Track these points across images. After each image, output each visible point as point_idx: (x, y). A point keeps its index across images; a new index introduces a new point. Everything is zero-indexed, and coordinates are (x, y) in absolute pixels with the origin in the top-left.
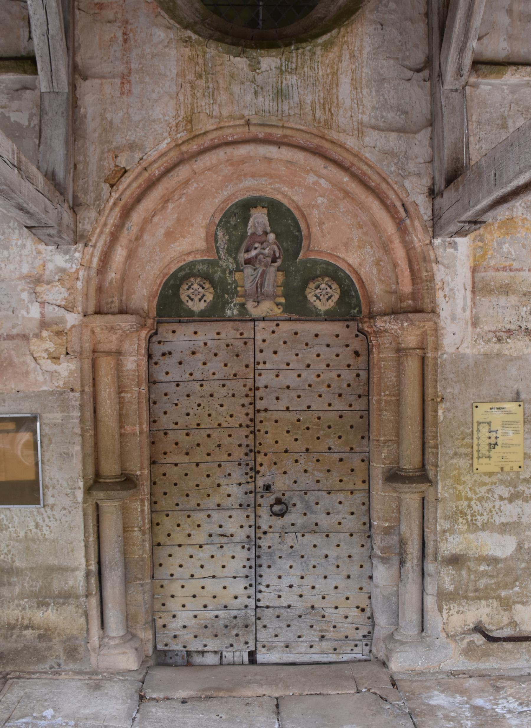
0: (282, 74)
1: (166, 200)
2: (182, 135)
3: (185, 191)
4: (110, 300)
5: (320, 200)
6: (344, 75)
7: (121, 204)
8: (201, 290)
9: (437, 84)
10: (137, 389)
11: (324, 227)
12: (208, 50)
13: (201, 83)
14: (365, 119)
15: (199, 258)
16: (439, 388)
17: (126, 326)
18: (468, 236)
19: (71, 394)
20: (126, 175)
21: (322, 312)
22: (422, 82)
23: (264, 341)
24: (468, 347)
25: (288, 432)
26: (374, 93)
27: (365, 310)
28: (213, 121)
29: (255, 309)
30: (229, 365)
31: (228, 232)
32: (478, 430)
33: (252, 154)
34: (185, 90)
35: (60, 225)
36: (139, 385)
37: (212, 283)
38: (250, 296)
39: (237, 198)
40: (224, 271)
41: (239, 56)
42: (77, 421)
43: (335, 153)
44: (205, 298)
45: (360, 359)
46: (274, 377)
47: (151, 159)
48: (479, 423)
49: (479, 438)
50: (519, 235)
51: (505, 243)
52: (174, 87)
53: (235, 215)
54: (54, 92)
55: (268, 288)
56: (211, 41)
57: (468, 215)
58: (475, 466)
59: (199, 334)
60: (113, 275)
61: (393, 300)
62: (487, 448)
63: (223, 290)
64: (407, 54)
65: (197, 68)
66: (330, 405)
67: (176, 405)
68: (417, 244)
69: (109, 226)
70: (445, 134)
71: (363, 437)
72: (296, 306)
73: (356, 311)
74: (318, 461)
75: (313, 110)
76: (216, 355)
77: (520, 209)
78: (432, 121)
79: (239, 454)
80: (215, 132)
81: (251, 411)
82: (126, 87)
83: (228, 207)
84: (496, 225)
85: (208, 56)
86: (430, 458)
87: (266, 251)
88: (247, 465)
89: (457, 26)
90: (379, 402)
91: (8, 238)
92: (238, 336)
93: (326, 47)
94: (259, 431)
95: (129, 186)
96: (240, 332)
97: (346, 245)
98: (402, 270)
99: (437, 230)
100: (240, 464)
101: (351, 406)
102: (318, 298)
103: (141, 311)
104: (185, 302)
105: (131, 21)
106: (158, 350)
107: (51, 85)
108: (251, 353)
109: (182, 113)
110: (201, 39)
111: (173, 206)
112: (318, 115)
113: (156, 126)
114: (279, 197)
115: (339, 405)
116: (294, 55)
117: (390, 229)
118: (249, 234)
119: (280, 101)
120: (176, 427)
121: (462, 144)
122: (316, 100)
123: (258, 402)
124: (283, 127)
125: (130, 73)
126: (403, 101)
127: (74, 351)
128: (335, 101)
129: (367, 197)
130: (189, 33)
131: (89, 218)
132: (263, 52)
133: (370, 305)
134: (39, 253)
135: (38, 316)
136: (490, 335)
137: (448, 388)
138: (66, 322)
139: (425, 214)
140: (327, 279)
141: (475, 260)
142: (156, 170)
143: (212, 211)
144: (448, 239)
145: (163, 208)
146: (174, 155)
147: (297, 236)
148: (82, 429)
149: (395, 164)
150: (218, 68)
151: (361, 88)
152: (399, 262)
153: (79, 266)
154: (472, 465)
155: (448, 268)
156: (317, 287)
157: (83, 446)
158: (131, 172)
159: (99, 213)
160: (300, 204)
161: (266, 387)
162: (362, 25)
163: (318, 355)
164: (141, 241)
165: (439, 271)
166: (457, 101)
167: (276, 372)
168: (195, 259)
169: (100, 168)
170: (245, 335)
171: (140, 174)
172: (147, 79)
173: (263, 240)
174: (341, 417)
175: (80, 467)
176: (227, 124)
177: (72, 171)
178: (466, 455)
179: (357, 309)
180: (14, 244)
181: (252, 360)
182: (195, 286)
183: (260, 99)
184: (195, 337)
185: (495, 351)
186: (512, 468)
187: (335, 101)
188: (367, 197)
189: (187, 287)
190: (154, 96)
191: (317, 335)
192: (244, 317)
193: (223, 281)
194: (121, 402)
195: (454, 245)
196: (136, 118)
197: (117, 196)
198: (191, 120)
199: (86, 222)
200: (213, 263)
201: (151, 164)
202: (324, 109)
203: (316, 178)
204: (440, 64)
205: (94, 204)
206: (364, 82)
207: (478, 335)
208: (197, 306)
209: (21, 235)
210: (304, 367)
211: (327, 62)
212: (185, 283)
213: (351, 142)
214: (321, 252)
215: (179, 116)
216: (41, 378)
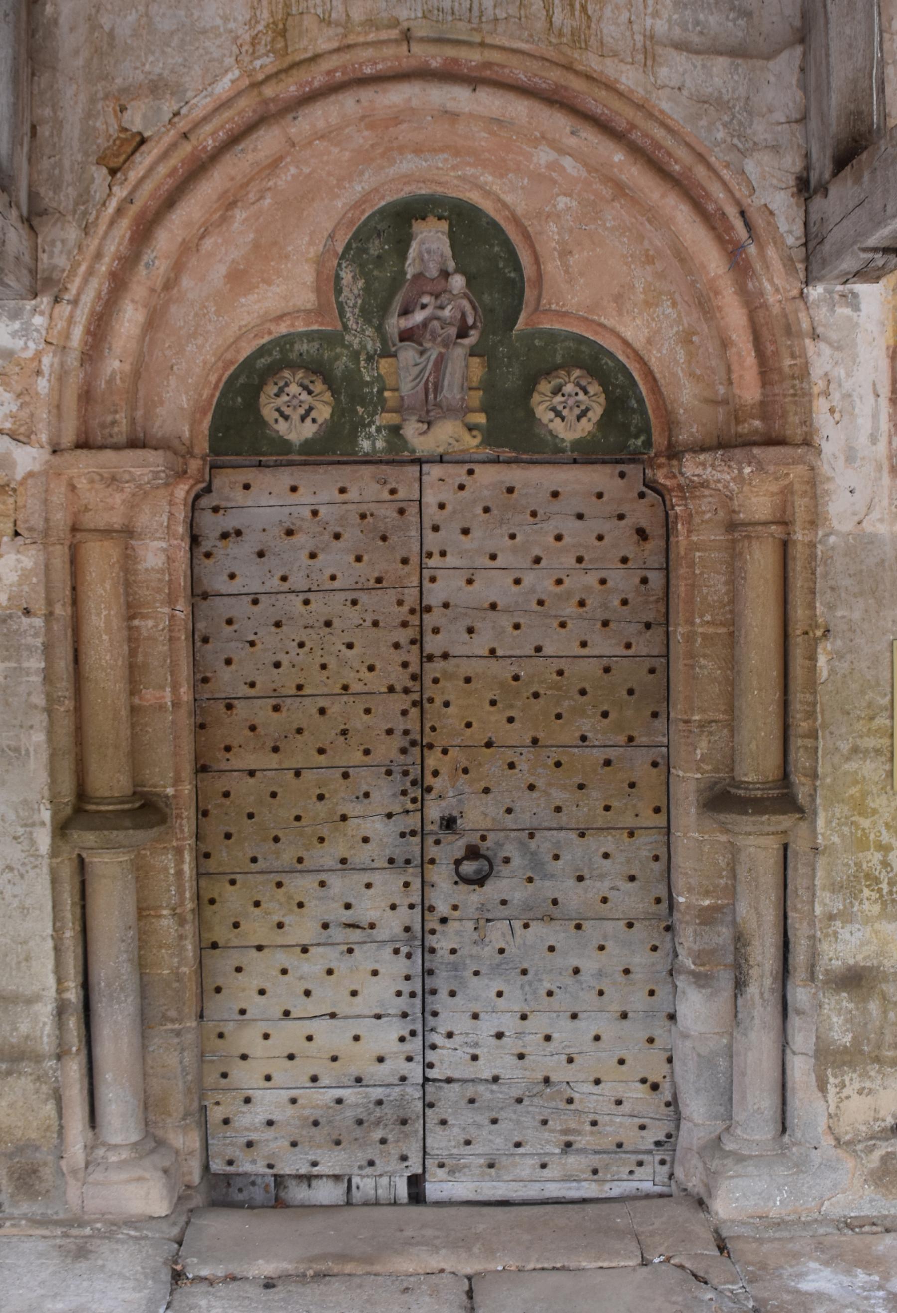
1: (229, 203)
2: (265, 63)
3: (271, 184)
4: (109, 418)
5: (562, 202)
7: (133, 210)
8: (305, 396)
10: (166, 610)
11: (571, 260)
14: (661, 27)
15: (301, 327)
16: (820, 609)
18: (883, 281)
19: (25, 621)
20: (144, 148)
21: (567, 445)
24: (881, 520)
25: (493, 703)
27: (659, 439)
28: (331, 32)
29: (422, 438)
30: (365, 558)
31: (363, 271)
36: (171, 601)
38: (411, 409)
39: (383, 198)
40: (355, 356)
43: (596, 101)
44: (313, 414)
45: (649, 546)
46: (464, 583)
47: (198, 113)
53: (379, 236)
55: (451, 392)
59: (301, 490)
60: (115, 365)
61: (720, 417)
63: (353, 398)
66: (584, 644)
67: (252, 644)
68: (772, 298)
69: (106, 259)
70: (832, 60)
71: (655, 715)
72: (512, 432)
73: (639, 442)
76: (337, 536)
80: (335, 57)
81: (413, 658)
83: (363, 218)
86: (800, 759)
87: (447, 313)
88: (405, 773)
90: (690, 638)
92: (386, 496)
94: (431, 700)
95: (149, 172)
96: (389, 487)
97: (619, 299)
98: (739, 354)
99: (815, 266)
100: (389, 773)
101: (628, 646)
102: (558, 414)
103: (176, 443)
104: (272, 422)
106: (211, 525)
108: (414, 533)
111: (244, 215)
112: (558, 18)
113: (208, 44)
114: (474, 197)
115: (604, 645)
117: (713, 265)
118: (409, 276)
120: (252, 692)
123: (428, 637)
124: (482, 45)
127: (31, 529)
129: (663, 196)
131: (63, 241)
133: (670, 430)
138: (13, 465)
139: (790, 232)
140: (577, 373)
143: (329, 226)
144: (839, 288)
145: (224, 219)
146: (246, 106)
147: (513, 281)
148: (50, 698)
149: (725, 125)
152: (734, 337)
153: (42, 346)
155: (839, 348)
156: (557, 391)
158: (153, 143)
159: (86, 230)
160: (519, 211)
161: (446, 606)
163: (559, 538)
164: (175, 291)
165: (819, 355)
167: (467, 574)
168: (292, 330)
169: (88, 134)
170: (401, 495)
171: (174, 146)
174: (607, 670)
175: (43, 778)
176: (361, 39)
177: (26, 139)
178: (878, 752)
179: (643, 438)
181: (416, 548)
182: (294, 389)
184: (294, 498)
188: (663, 196)
189: (275, 389)
191: (555, 495)
192: (398, 455)
193: (352, 377)
194: (133, 638)
195: (852, 300)
196: (165, 25)
198: (285, 30)
201: (197, 125)
203: (552, 156)
205: (75, 212)
208: (296, 432)
210: (528, 563)
212: (270, 382)
213: (629, 78)
214: (565, 314)
215: (257, 22)
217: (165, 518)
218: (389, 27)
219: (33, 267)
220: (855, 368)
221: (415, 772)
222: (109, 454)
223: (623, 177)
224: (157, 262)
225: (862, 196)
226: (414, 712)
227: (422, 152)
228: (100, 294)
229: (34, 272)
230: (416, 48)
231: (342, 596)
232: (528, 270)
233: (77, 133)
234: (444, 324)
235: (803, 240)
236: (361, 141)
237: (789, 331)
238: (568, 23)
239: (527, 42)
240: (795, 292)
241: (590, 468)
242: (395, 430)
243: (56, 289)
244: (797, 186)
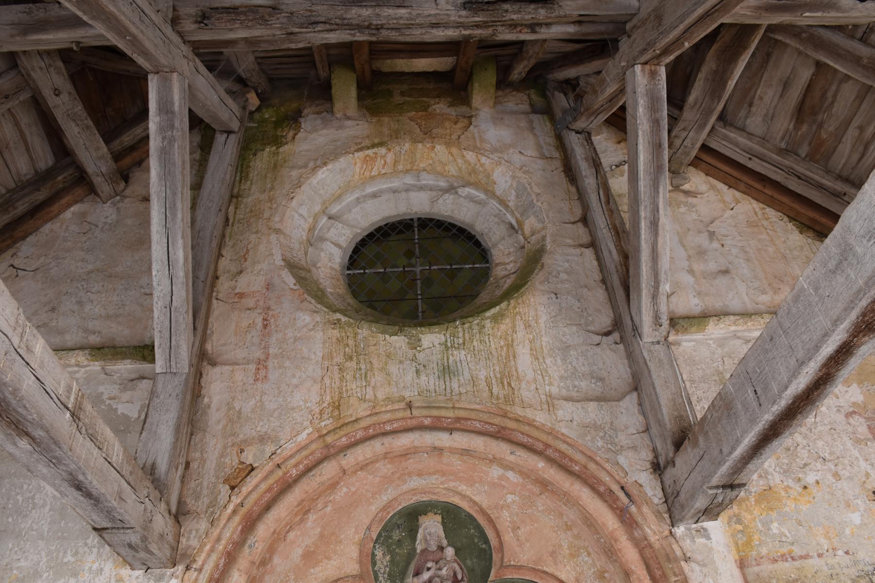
0: (447, 350)
1: (304, 510)
2: (327, 423)
5: (510, 498)
6: (521, 346)
7: (243, 511)
9: (634, 340)
11: (520, 532)
12: (360, 331)
13: (352, 364)
14: (554, 390)
18: (720, 519)
20: (253, 473)
22: (613, 345)
26: (559, 362)
28: (366, 405)
31: (389, 551)
33: (417, 444)
34: (332, 373)
41: (396, 335)
47: (287, 453)
50: (787, 509)
51: (772, 522)
53: (398, 527)
54: (171, 372)
56: (363, 322)
64: (590, 319)
65: (347, 349)
68: (653, 539)
69: (223, 542)
70: (658, 390)
75: (489, 386)
77: (776, 474)
78: (638, 384)
80: (368, 419)
82: (262, 373)
83: (389, 517)
85: (360, 337)
87: (444, 572)
89: (644, 270)
91: (81, 561)
93: (495, 319)
95: (254, 488)
99: (676, 513)
105: (273, 308)
107: (168, 364)
109: (328, 399)
110: (351, 320)
111: (314, 517)
112: (495, 390)
113: (294, 415)
114: (456, 500)
116: (460, 329)
117: (610, 523)
118: (418, 551)
119: (447, 378)
121: (682, 400)
122: (492, 375)
124: (454, 408)
125: (267, 358)
126: (596, 367)
128: (515, 373)
129: (572, 484)
130: (338, 316)
131: (197, 530)
132: (423, 329)
139: (654, 495)
141: (738, 551)
143: (367, 522)
144: (694, 526)
145: (302, 520)
147: (485, 550)
150: (372, 348)
151: (544, 358)
152: (633, 567)
155: (704, 565)
162: (534, 295)
164: (269, 566)
165: (692, 571)
166: (662, 354)
169: (220, 466)
171: (271, 472)
172: (287, 364)
173: (438, 557)
176: (384, 409)
180: (87, 568)
183: (423, 378)
187: (515, 373)
188: (572, 484)
190: (295, 381)
196: (270, 406)
197: (239, 501)
198: (339, 405)
199: (192, 536)
201: (286, 460)
202: (502, 383)
204: (631, 317)
205: (206, 512)
206: (545, 351)
209: (99, 555)
211: (499, 334)
213: (541, 418)
215: (324, 402)
218: (399, 401)
219: (175, 546)
220: (718, 577)
223: (545, 476)
224: (257, 545)
225: (701, 453)
227: (422, 475)
228: (218, 566)
230: (416, 412)
233: (214, 465)
235: (664, 500)
236: (386, 471)
237: (670, 558)
238: (502, 393)
239: (479, 404)
240: (667, 533)
243: (188, 561)
244: (652, 467)
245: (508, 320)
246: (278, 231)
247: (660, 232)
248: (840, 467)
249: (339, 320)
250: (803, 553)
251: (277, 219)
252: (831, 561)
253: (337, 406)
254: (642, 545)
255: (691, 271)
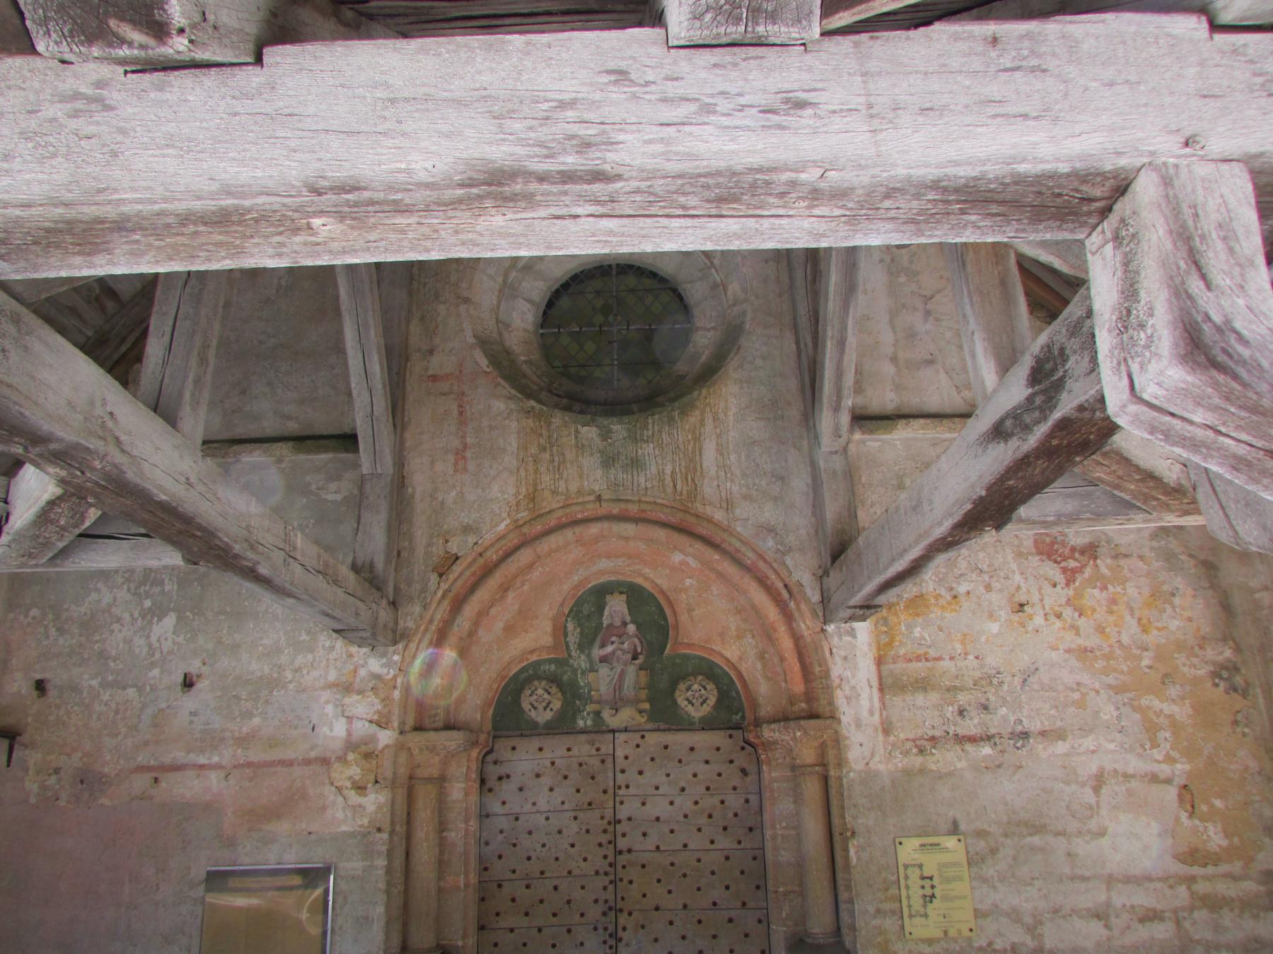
1: (505, 588)
2: (524, 515)
5: (688, 582)
7: (451, 595)
8: (546, 696)
10: (463, 826)
16: (848, 818)
17: (452, 745)
19: (378, 835)
23: (626, 758)
24: (880, 762)
25: (659, 881)
27: (748, 714)
32: (907, 877)
35: (374, 626)
36: (467, 821)
37: (560, 686)
42: (381, 872)
43: (703, 530)
45: (748, 779)
47: (487, 543)
48: (906, 867)
49: (907, 887)
50: (932, 615)
52: (515, 462)
57: (857, 599)
58: (908, 929)
59: (545, 750)
62: (921, 901)
63: (573, 695)
66: (712, 842)
67: (514, 845)
71: (758, 887)
72: (663, 712)
74: (700, 922)
77: (931, 583)
79: (594, 912)
81: (610, 851)
82: (461, 463)
84: (902, 605)
86: (845, 917)
87: (626, 646)
88: (606, 929)
90: (774, 838)
92: (594, 752)
94: (621, 880)
99: (827, 613)
100: (595, 929)
101: (739, 842)
102: (690, 702)
106: (493, 771)
108: (611, 775)
115: (725, 843)
120: (513, 876)
123: (619, 839)
127: (384, 779)
130: (533, 403)
134: (351, 656)
135: (343, 734)
136: (909, 745)
137: (860, 817)
138: (377, 740)
140: (700, 678)
141: (879, 649)
142: (492, 555)
145: (503, 597)
146: (514, 540)
148: (389, 884)
154: (903, 927)
156: (688, 689)
157: (388, 906)
159: (425, 607)
160: (665, 587)
161: (630, 819)
163: (695, 775)
170: (603, 751)
171: (475, 560)
174: (727, 858)
175: (381, 937)
177: (394, 560)
178: (893, 912)
181: (611, 783)
182: (540, 691)
184: (540, 755)
185: (917, 765)
186: (959, 931)
190: (492, 472)
191: (692, 749)
192: (599, 729)
193: (574, 684)
194: (442, 843)
195: (852, 633)
196: (471, 497)
200: (561, 663)
201: (486, 549)
203: (682, 557)
206: (731, 447)
207: (893, 745)
213: (719, 516)
214: (693, 645)
216: (340, 815)
217: (464, 769)
221: (611, 928)
222: (432, 733)
226: (611, 887)
229: (394, 631)
231: (568, 815)
232: (671, 619)
234: (624, 652)
240: (818, 629)
241: (710, 732)
242: (597, 714)
245: (697, 412)
246: (467, 300)
247: (847, 350)
248: (994, 579)
249: (533, 408)
250: (938, 655)
251: (464, 285)
252: (960, 664)
253: (532, 498)
254: (797, 638)
255: (894, 360)
